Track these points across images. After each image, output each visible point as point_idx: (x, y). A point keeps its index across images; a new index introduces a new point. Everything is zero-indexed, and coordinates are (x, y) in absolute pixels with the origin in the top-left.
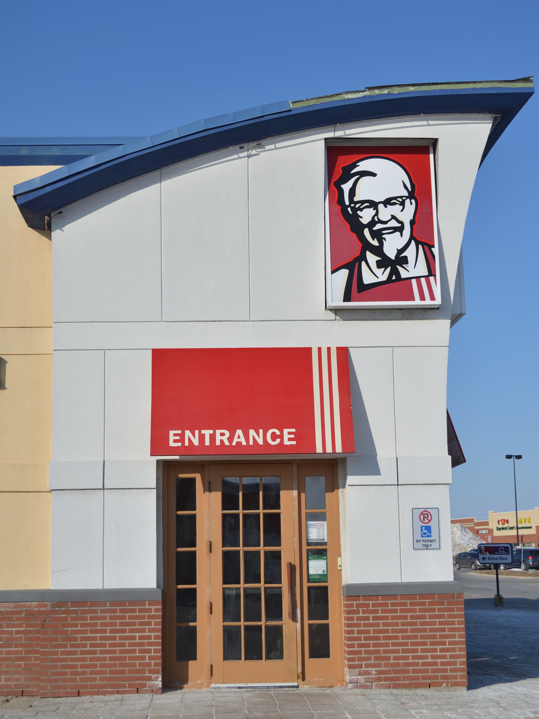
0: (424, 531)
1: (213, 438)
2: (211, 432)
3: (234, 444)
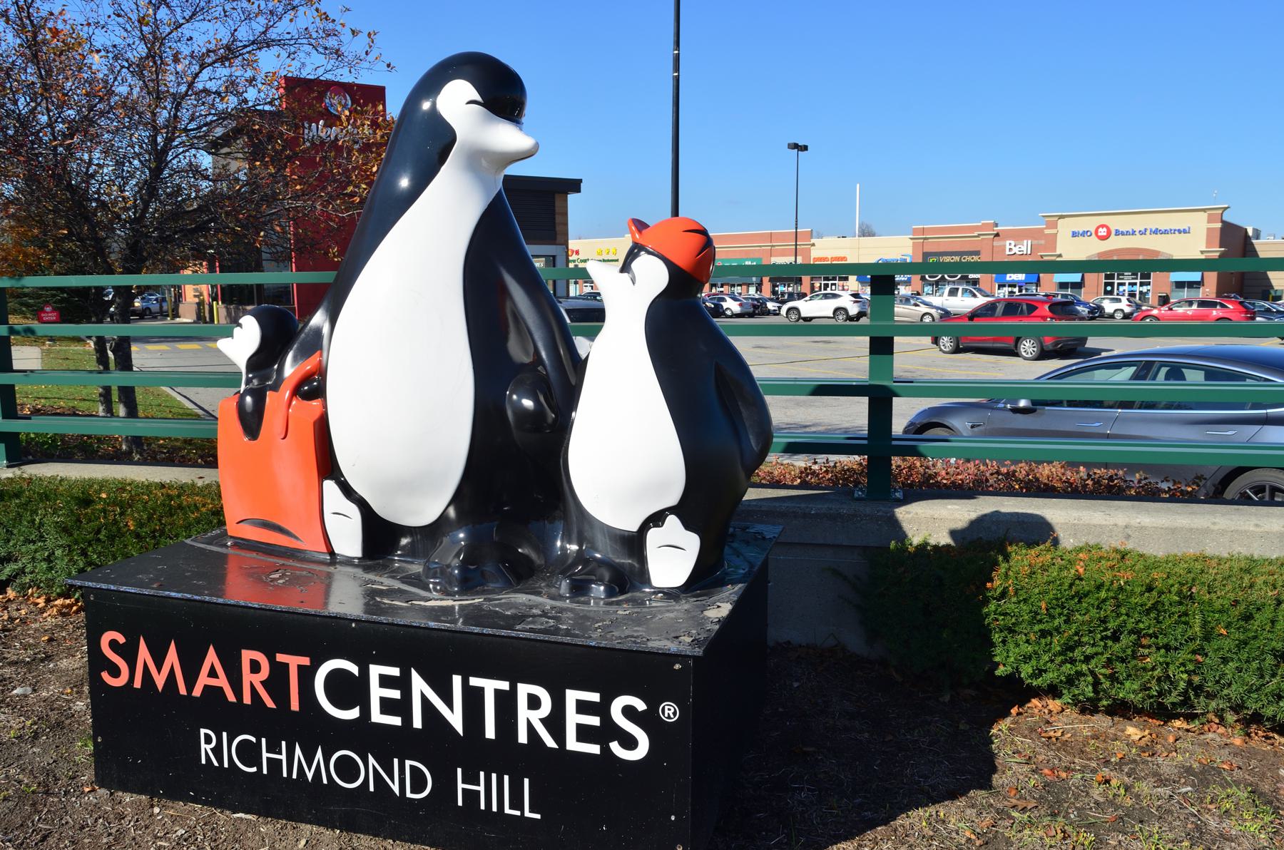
2: (305, 661)
3: (197, 692)
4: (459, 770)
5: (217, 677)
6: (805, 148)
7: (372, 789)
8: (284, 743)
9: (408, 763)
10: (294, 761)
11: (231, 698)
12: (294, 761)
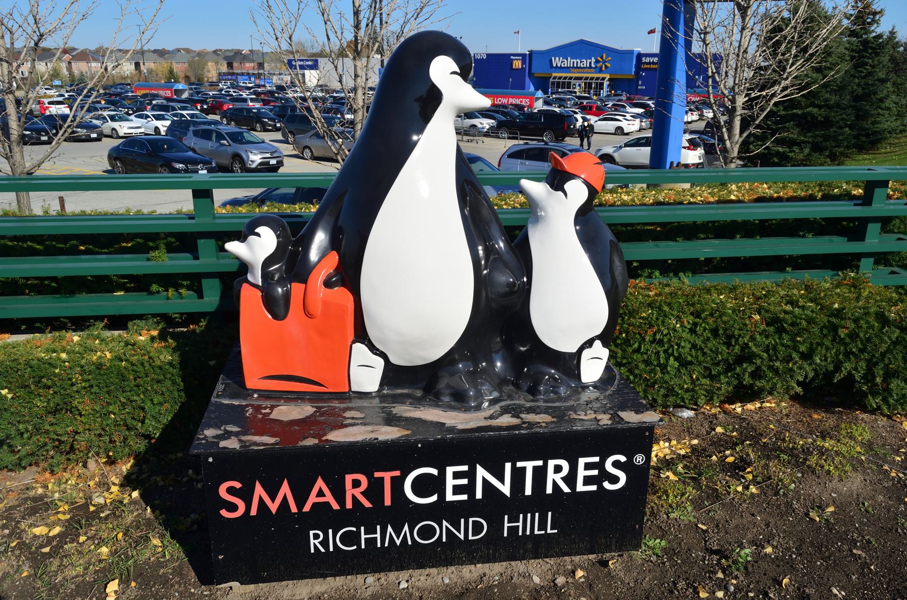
1: (540, 474)
2: (397, 473)
3: (307, 508)
4: (550, 513)
5: (317, 496)
6: (649, 33)
7: (444, 540)
8: (378, 527)
9: (471, 520)
10: (387, 536)
11: (336, 506)
12: (387, 536)
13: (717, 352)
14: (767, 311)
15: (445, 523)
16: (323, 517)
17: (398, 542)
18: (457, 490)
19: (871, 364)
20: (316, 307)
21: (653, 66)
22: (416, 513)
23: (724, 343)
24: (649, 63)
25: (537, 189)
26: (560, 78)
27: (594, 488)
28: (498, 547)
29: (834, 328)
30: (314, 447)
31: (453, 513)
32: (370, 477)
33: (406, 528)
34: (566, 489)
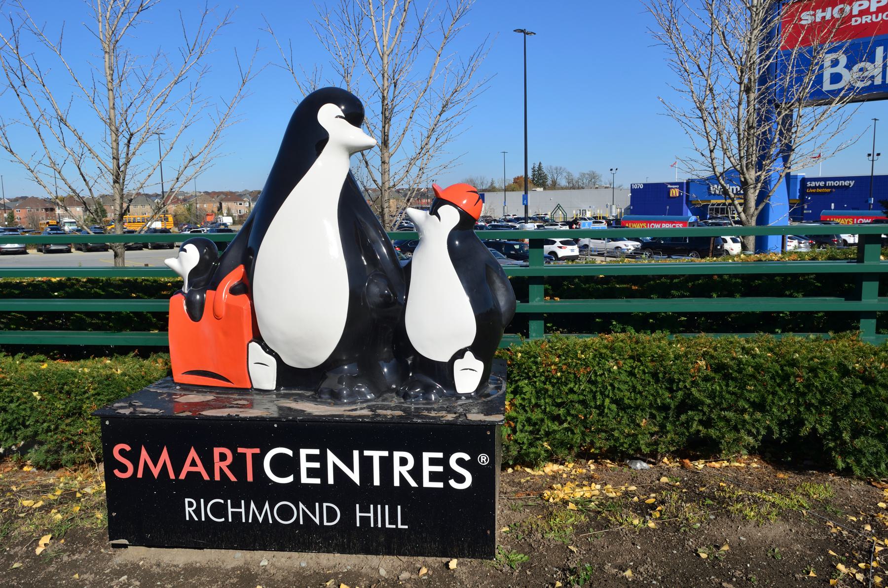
0: (219, 254)
1: (387, 465)
2: (257, 451)
3: (182, 476)
4: (399, 507)
5: (191, 465)
7: (301, 523)
9: (325, 505)
11: (206, 477)
13: (656, 395)
14: (712, 357)
15: (301, 505)
16: (197, 487)
17: (260, 519)
18: (311, 473)
19: (835, 418)
20: (222, 311)
21: (818, 190)
22: (275, 493)
23: (667, 388)
24: (815, 187)
25: (417, 215)
26: (719, 205)
27: (440, 485)
28: (353, 539)
29: (786, 377)
30: (188, 417)
31: (309, 495)
32: (234, 452)
33: (267, 506)
34: (413, 484)
